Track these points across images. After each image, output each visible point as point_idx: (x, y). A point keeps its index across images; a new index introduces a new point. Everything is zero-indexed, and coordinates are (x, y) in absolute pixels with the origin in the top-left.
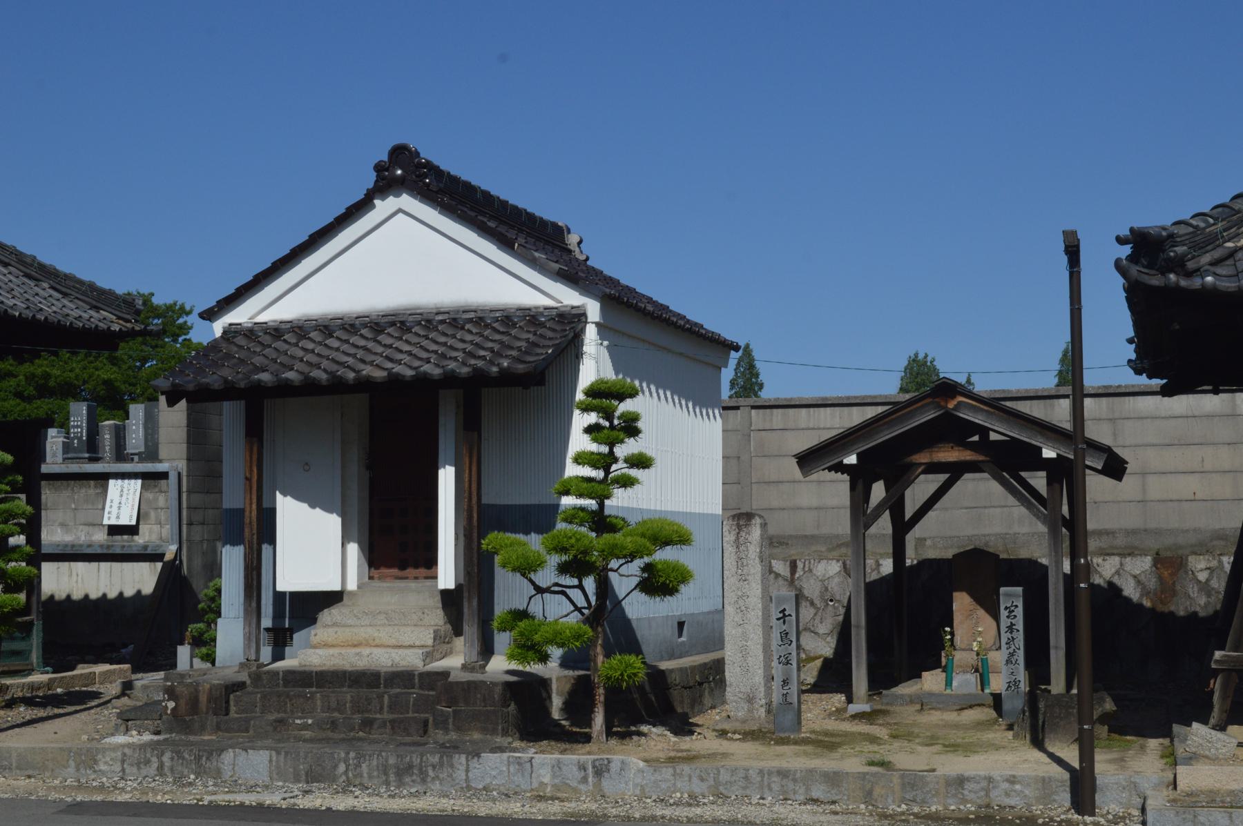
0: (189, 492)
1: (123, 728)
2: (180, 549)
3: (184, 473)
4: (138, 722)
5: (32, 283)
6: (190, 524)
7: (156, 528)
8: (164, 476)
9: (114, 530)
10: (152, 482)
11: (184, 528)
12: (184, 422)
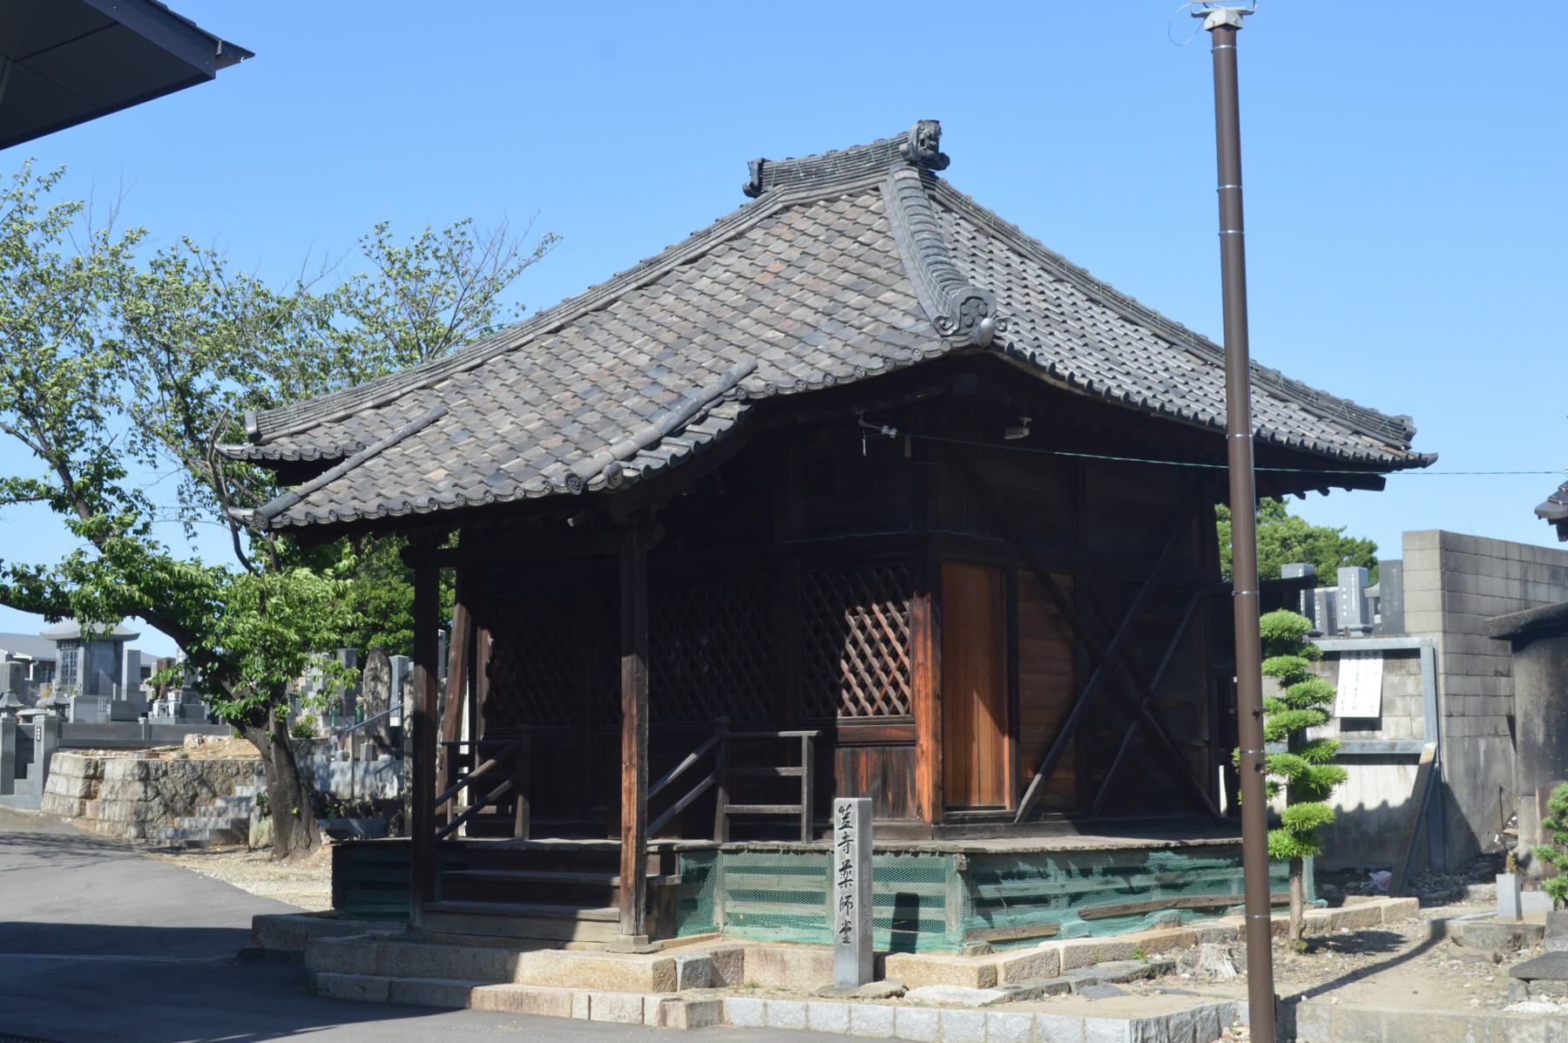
0: (1447, 674)
1: (1521, 990)
2: (1439, 747)
3: (1440, 650)
4: (1544, 983)
5: (1281, 405)
6: (1450, 715)
7: (1405, 721)
8: (1414, 653)
9: (1350, 724)
10: (1396, 662)
11: (1443, 720)
12: (1438, 584)
